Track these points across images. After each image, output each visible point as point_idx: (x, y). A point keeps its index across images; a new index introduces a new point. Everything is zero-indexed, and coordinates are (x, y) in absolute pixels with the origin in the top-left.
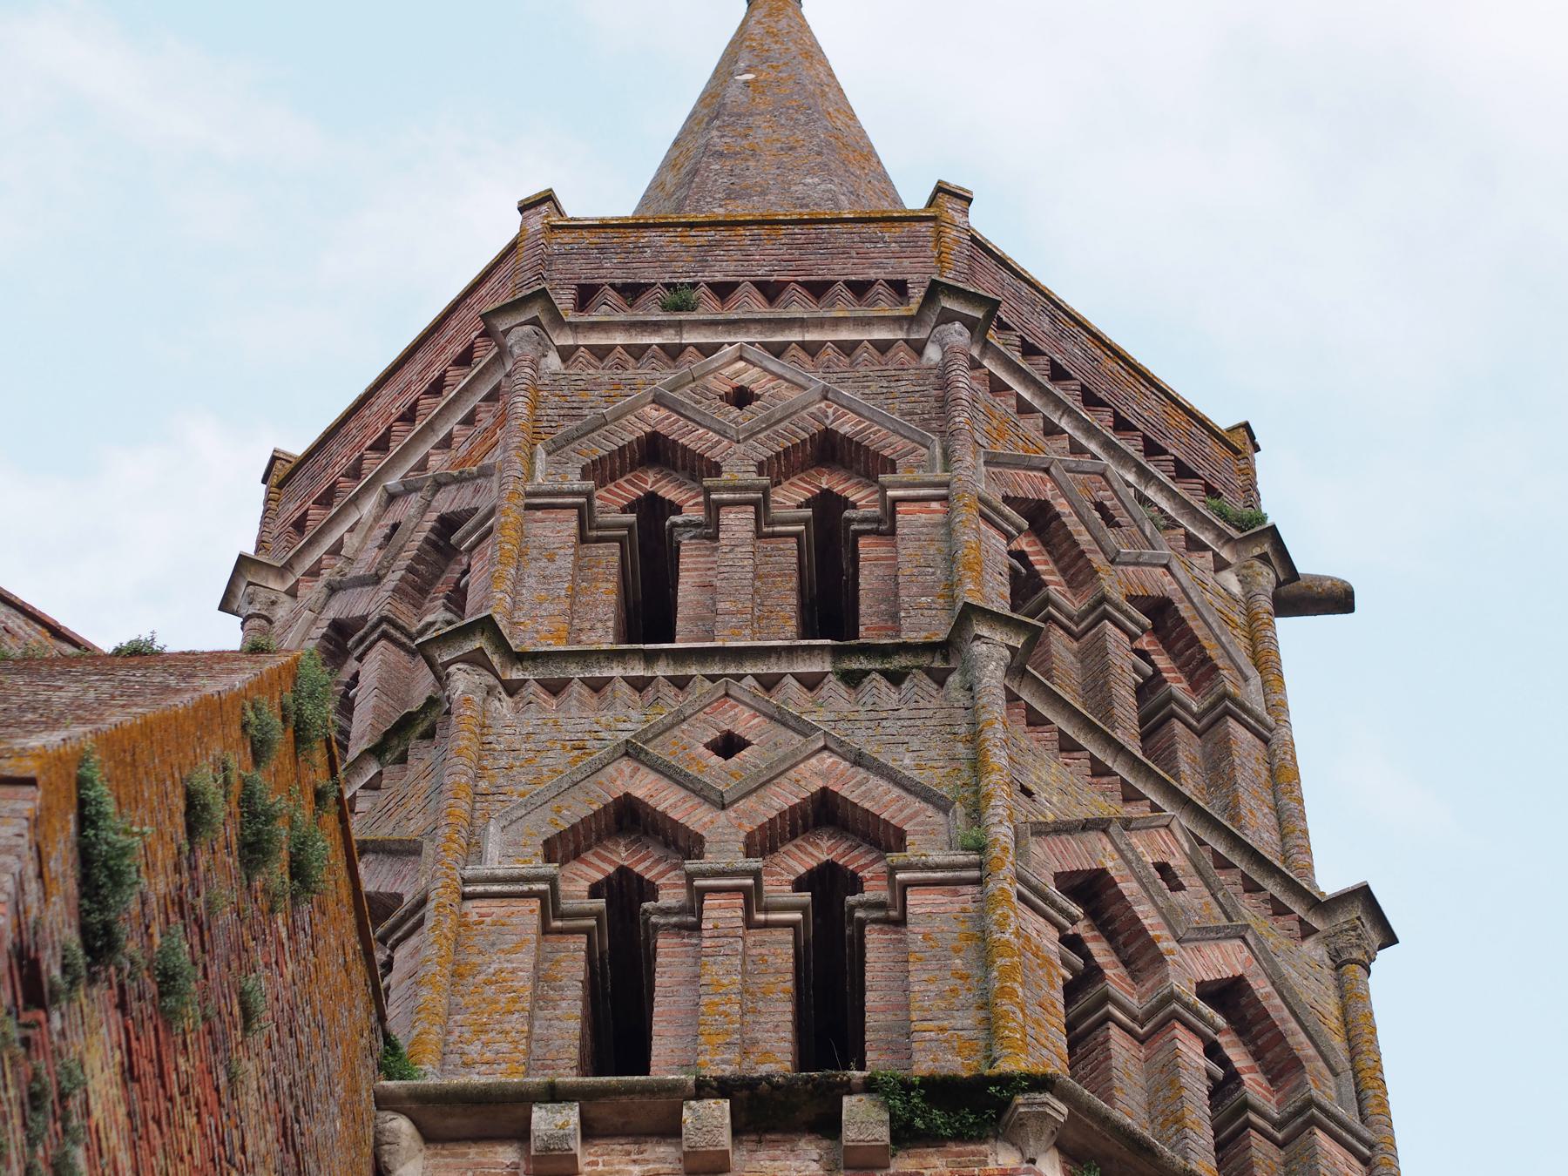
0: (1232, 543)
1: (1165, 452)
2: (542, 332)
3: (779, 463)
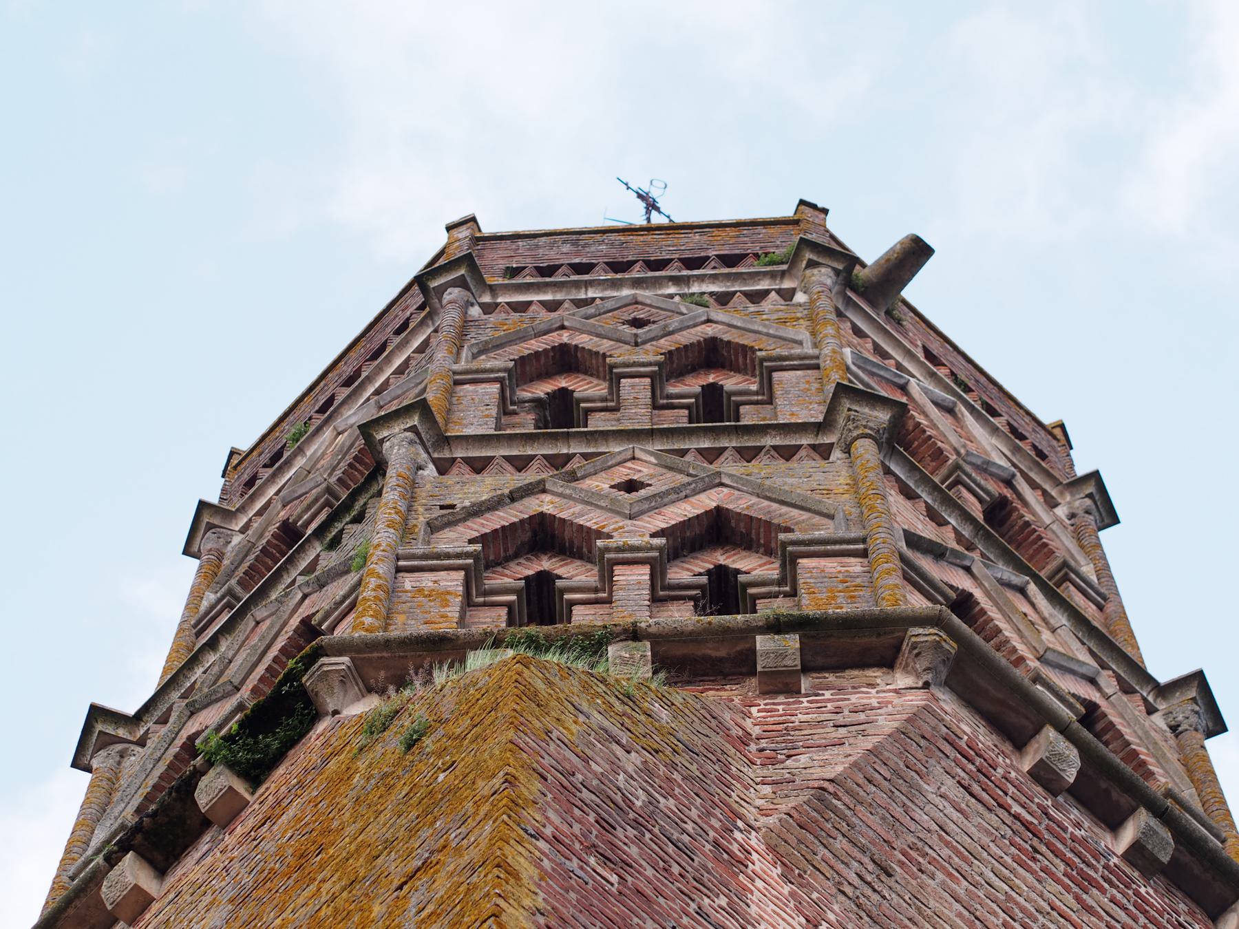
0: (787, 275)
1: (708, 258)
2: (218, 529)
3: (357, 470)
